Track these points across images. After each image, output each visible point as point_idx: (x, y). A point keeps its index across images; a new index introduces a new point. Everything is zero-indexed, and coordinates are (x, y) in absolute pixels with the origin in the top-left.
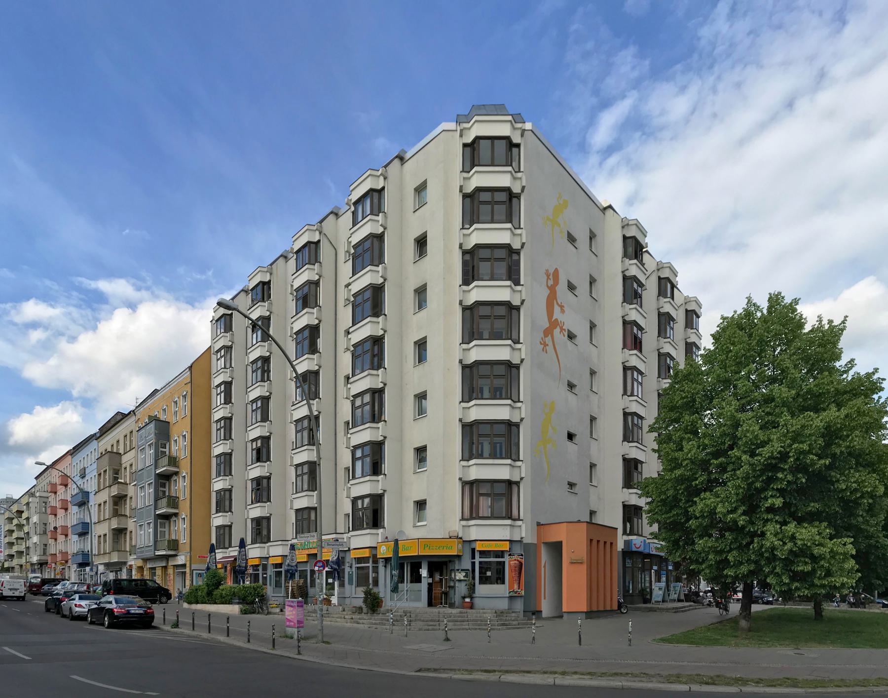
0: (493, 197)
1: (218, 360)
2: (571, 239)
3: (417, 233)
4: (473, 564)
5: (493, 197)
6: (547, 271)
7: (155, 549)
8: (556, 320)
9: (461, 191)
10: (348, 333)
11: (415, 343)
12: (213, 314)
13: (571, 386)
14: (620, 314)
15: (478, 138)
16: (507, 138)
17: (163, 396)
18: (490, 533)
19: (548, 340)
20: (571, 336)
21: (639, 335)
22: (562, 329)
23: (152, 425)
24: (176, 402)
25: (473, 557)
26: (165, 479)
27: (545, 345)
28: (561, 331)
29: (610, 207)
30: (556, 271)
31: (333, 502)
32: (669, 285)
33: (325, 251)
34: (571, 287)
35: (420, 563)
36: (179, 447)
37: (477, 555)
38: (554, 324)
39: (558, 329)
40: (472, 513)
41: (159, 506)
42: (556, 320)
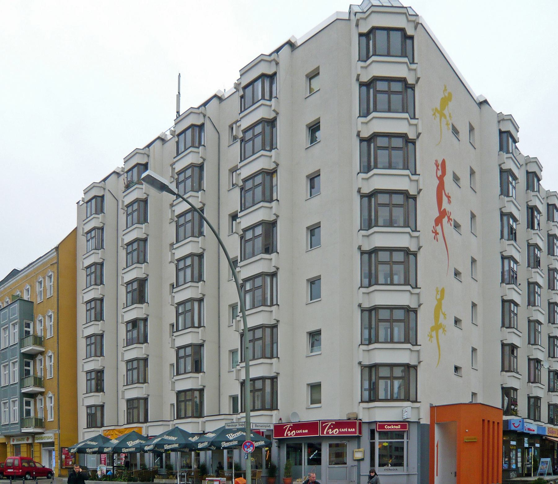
0: (389, 87)
1: (88, 241)
2: (455, 131)
3: (310, 119)
4: (372, 446)
5: (389, 87)
6: (437, 161)
7: (22, 426)
8: (445, 209)
9: (358, 79)
10: (234, 217)
11: (308, 228)
12: (83, 196)
13: (457, 274)
14: (498, 207)
15: (374, 29)
16: (402, 30)
17: (27, 276)
18: (386, 413)
19: (439, 229)
20: (457, 226)
21: (514, 227)
22: (449, 219)
23: (17, 305)
24: (40, 283)
25: (373, 437)
26: (29, 357)
27: (437, 233)
28: (449, 221)
29: (486, 102)
30: (444, 162)
31: (217, 384)
32: (536, 180)
33: (209, 134)
34: (456, 179)
35: (301, 444)
36: (45, 325)
37: (377, 435)
38: (443, 213)
39: (442, 329)
40: (372, 396)
41: (26, 385)
42: (445, 209)
